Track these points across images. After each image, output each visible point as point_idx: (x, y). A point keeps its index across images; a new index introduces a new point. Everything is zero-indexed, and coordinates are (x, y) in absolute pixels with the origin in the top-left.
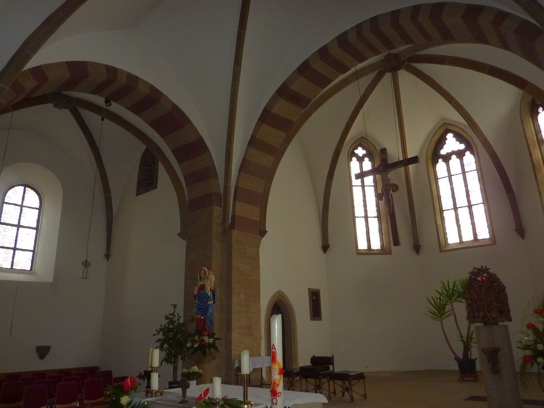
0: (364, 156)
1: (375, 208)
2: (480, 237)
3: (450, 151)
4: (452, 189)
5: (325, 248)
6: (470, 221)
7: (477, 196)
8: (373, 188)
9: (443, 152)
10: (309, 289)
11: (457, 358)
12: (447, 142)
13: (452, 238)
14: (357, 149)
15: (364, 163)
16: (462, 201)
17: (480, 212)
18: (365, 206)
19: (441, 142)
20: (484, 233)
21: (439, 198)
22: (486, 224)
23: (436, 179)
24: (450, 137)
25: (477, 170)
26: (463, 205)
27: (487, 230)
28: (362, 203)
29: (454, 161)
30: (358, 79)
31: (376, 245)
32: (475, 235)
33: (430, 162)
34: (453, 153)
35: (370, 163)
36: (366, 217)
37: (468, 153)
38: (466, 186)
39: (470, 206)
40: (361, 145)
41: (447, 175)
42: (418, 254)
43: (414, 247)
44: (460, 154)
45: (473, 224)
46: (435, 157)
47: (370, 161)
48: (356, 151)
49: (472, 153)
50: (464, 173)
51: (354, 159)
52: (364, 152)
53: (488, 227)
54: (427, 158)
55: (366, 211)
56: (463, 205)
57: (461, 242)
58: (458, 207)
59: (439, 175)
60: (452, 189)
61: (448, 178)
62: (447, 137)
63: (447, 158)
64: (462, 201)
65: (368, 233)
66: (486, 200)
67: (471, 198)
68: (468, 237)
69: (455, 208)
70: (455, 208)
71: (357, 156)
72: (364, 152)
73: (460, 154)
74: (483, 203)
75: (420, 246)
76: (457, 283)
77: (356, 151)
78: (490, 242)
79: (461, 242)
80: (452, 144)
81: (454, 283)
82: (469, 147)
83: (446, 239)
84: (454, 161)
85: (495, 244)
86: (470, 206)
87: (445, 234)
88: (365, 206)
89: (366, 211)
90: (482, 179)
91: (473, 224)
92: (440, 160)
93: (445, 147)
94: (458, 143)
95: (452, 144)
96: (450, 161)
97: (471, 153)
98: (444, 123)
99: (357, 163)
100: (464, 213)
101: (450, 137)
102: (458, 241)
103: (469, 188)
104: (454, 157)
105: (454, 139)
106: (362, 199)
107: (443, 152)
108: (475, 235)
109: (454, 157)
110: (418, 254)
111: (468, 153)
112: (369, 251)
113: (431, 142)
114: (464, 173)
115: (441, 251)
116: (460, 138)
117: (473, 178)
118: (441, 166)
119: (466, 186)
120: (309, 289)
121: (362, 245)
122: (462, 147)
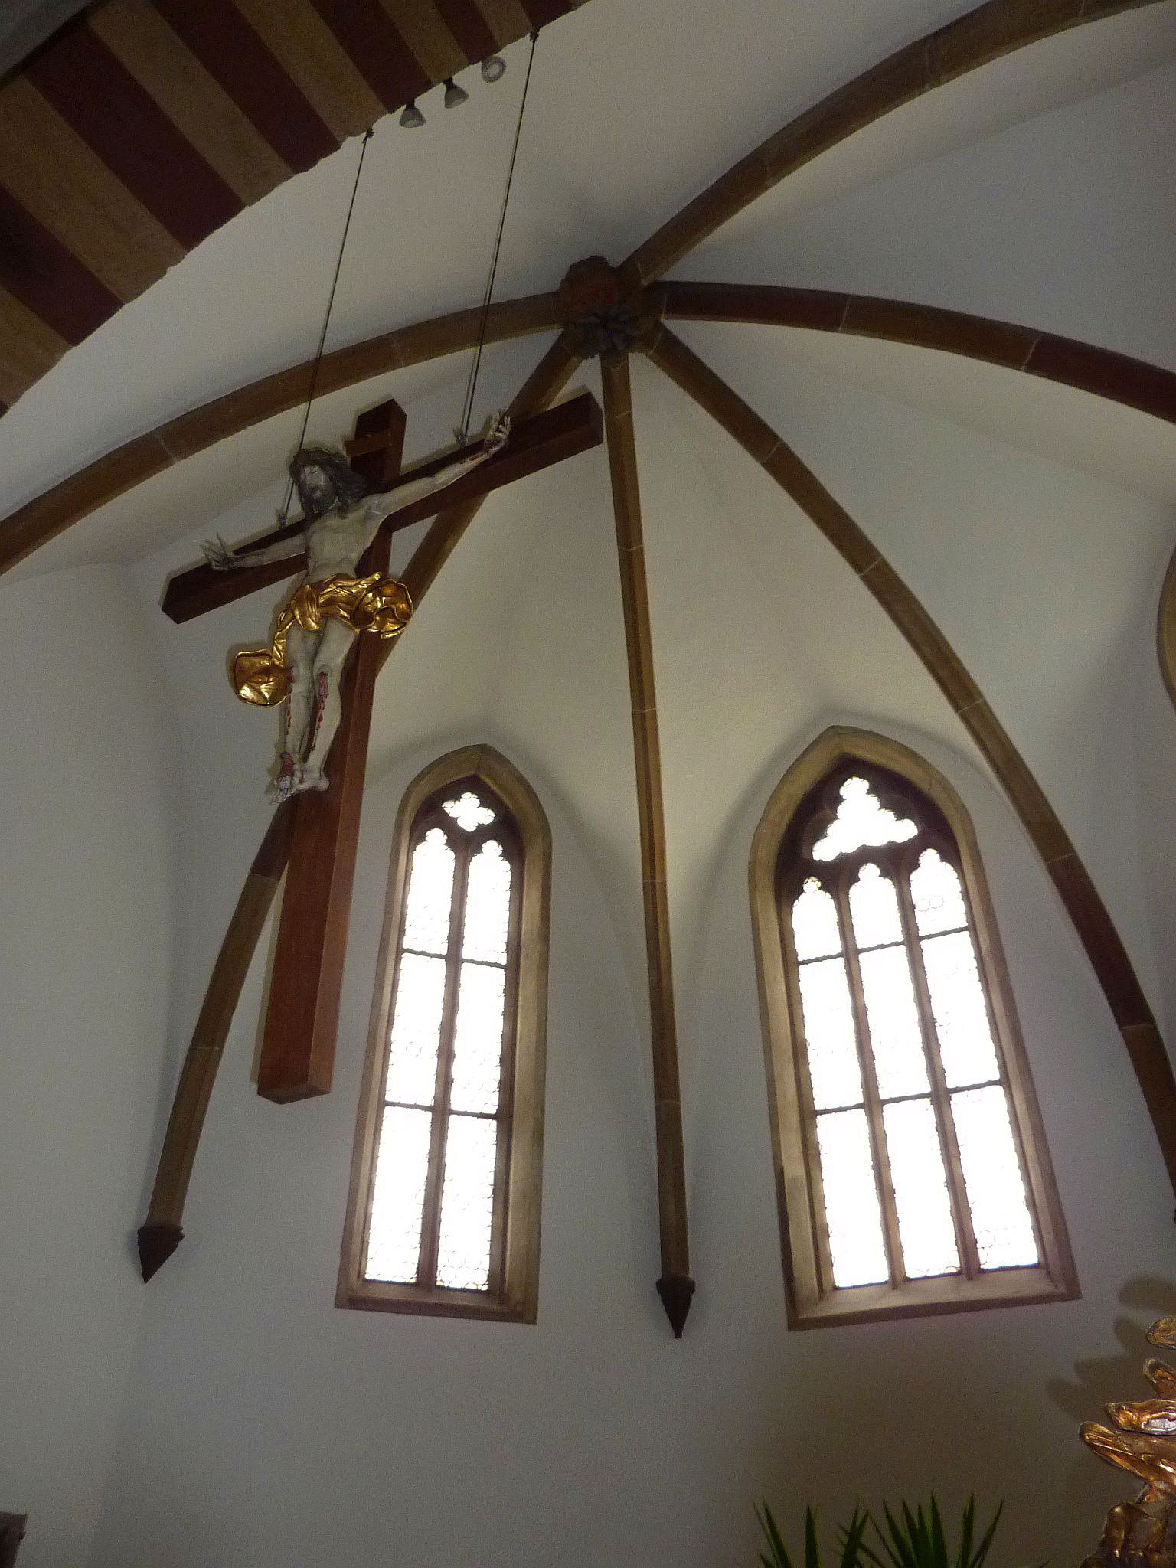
0: (483, 834)
1: (493, 1073)
2: (990, 1258)
3: (850, 848)
4: (860, 1015)
5: (155, 1244)
6: (940, 1173)
7: (972, 1049)
8: (499, 976)
9: (824, 851)
10: (21, 1520)
11: (534, 37)
12: (841, 810)
13: (855, 1263)
14: (456, 797)
15: (477, 863)
16: (901, 1069)
17: (988, 1124)
18: (446, 1054)
19: (816, 808)
20: (1010, 1241)
21: (799, 1050)
22: (1020, 1191)
23: (791, 964)
24: (855, 791)
25: (972, 928)
26: (917, 1127)
27: (1026, 1219)
28: (435, 1040)
29: (872, 889)
30: (480, 340)
31: (466, 1265)
32: (967, 1244)
33: (766, 883)
34: (865, 855)
35: (507, 865)
36: (441, 1111)
37: (930, 858)
38: (923, 998)
39: (940, 1096)
40: (473, 784)
41: (838, 948)
42: (678, 1334)
43: (661, 1286)
44: (897, 863)
45: (956, 1186)
46: (789, 864)
47: (506, 855)
48: (451, 808)
49: (951, 855)
50: (912, 940)
51: (436, 837)
52: (487, 816)
53: (1032, 1203)
54: (753, 864)
55: (445, 1081)
56: (917, 1127)
57: (898, 1280)
58: (884, 1095)
59: (803, 948)
60: (860, 1015)
61: (841, 961)
62: (843, 791)
63: (839, 877)
64: (901, 1069)
65: (429, 1192)
66: (1018, 1070)
67: (947, 1057)
68: (931, 1255)
69: (872, 1104)
70: (872, 1104)
71: (449, 825)
72: (487, 816)
73: (897, 863)
74: (1004, 1081)
75: (690, 1287)
76: (869, 1537)
77: (451, 808)
78: (1043, 1286)
79: (898, 1280)
80: (861, 819)
81: (854, 1536)
82: (939, 831)
83: (822, 1261)
84: (872, 889)
85: (1072, 1292)
86: (940, 1096)
87: (819, 1233)
88: (446, 1054)
89: (445, 1081)
90: (995, 968)
91: (956, 1186)
92: (812, 885)
93: (832, 829)
94: (890, 815)
95: (861, 819)
96: (855, 891)
97: (944, 858)
98: (835, 731)
99: (447, 858)
100: (911, 1128)
101: (855, 791)
102: (882, 1274)
103: (937, 1009)
104: (869, 873)
105: (874, 801)
106: (437, 1015)
107: (824, 851)
108: (967, 1244)
109: (869, 873)
110: (678, 1334)
111: (930, 858)
112: (424, 1295)
113: (774, 797)
114: (912, 940)
115: (795, 1323)
116: (896, 791)
117: (954, 965)
118: (812, 909)
119: (923, 998)
120: (21, 1520)
121: (390, 1259)
122: (906, 830)
